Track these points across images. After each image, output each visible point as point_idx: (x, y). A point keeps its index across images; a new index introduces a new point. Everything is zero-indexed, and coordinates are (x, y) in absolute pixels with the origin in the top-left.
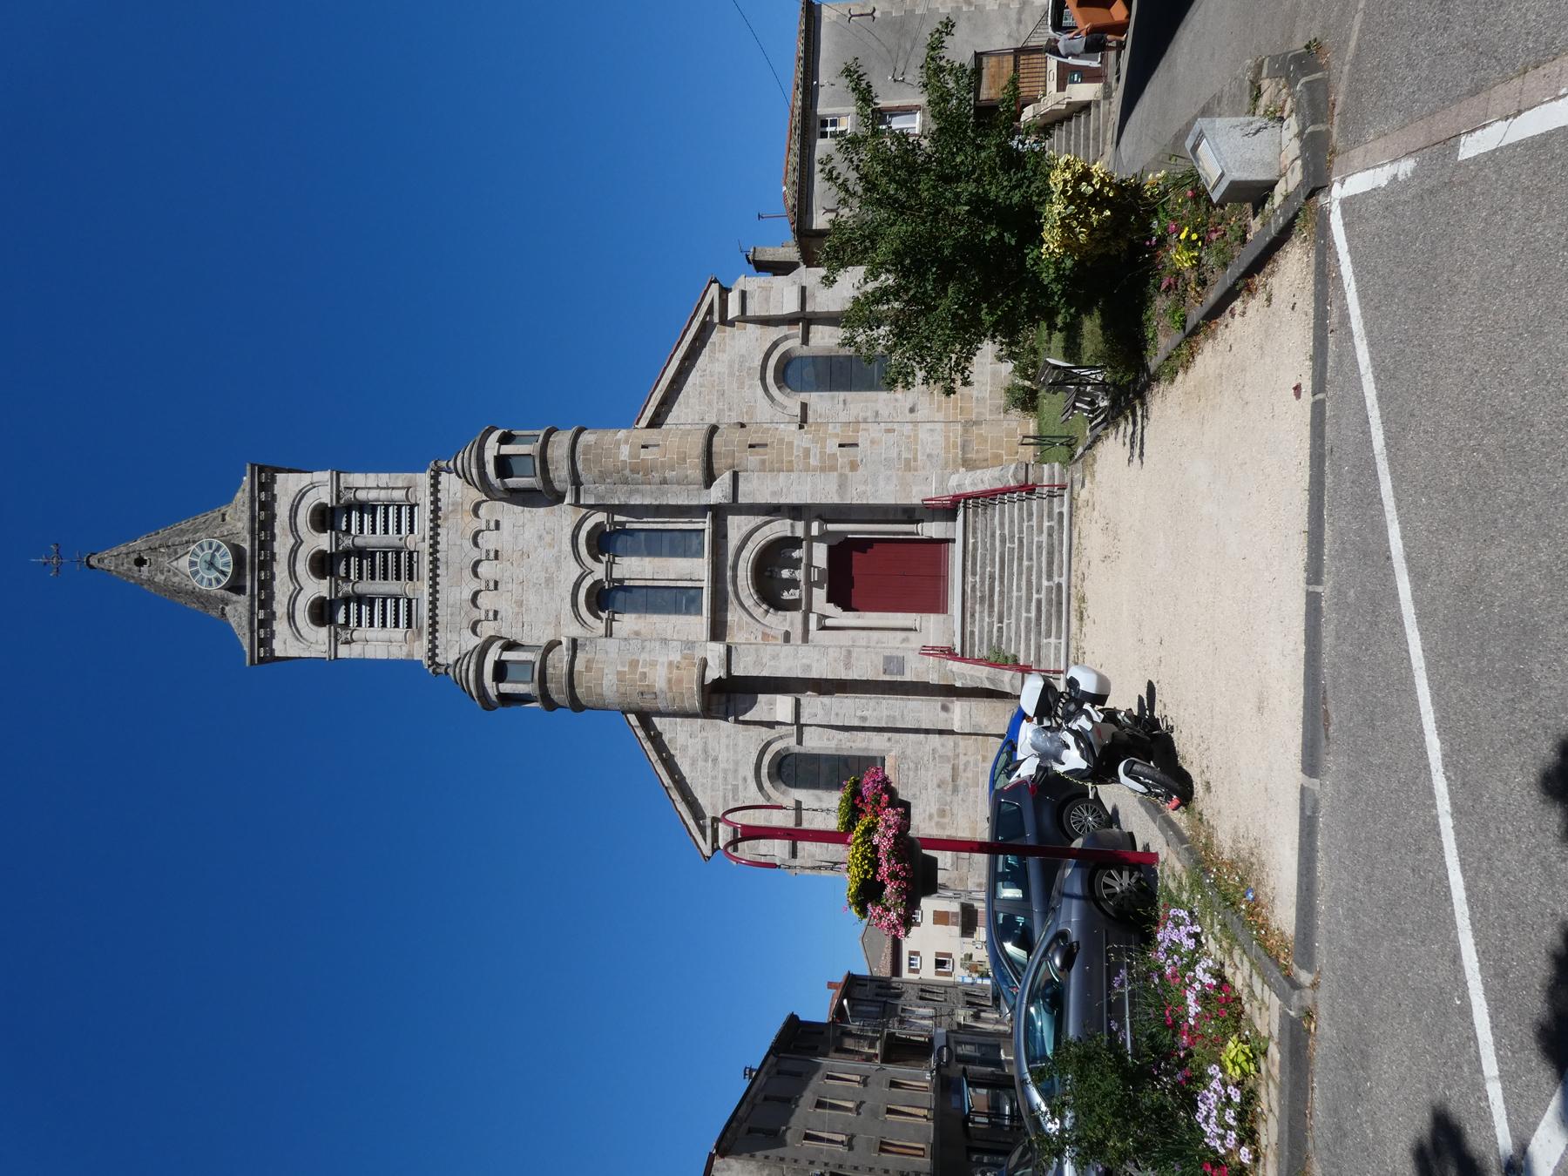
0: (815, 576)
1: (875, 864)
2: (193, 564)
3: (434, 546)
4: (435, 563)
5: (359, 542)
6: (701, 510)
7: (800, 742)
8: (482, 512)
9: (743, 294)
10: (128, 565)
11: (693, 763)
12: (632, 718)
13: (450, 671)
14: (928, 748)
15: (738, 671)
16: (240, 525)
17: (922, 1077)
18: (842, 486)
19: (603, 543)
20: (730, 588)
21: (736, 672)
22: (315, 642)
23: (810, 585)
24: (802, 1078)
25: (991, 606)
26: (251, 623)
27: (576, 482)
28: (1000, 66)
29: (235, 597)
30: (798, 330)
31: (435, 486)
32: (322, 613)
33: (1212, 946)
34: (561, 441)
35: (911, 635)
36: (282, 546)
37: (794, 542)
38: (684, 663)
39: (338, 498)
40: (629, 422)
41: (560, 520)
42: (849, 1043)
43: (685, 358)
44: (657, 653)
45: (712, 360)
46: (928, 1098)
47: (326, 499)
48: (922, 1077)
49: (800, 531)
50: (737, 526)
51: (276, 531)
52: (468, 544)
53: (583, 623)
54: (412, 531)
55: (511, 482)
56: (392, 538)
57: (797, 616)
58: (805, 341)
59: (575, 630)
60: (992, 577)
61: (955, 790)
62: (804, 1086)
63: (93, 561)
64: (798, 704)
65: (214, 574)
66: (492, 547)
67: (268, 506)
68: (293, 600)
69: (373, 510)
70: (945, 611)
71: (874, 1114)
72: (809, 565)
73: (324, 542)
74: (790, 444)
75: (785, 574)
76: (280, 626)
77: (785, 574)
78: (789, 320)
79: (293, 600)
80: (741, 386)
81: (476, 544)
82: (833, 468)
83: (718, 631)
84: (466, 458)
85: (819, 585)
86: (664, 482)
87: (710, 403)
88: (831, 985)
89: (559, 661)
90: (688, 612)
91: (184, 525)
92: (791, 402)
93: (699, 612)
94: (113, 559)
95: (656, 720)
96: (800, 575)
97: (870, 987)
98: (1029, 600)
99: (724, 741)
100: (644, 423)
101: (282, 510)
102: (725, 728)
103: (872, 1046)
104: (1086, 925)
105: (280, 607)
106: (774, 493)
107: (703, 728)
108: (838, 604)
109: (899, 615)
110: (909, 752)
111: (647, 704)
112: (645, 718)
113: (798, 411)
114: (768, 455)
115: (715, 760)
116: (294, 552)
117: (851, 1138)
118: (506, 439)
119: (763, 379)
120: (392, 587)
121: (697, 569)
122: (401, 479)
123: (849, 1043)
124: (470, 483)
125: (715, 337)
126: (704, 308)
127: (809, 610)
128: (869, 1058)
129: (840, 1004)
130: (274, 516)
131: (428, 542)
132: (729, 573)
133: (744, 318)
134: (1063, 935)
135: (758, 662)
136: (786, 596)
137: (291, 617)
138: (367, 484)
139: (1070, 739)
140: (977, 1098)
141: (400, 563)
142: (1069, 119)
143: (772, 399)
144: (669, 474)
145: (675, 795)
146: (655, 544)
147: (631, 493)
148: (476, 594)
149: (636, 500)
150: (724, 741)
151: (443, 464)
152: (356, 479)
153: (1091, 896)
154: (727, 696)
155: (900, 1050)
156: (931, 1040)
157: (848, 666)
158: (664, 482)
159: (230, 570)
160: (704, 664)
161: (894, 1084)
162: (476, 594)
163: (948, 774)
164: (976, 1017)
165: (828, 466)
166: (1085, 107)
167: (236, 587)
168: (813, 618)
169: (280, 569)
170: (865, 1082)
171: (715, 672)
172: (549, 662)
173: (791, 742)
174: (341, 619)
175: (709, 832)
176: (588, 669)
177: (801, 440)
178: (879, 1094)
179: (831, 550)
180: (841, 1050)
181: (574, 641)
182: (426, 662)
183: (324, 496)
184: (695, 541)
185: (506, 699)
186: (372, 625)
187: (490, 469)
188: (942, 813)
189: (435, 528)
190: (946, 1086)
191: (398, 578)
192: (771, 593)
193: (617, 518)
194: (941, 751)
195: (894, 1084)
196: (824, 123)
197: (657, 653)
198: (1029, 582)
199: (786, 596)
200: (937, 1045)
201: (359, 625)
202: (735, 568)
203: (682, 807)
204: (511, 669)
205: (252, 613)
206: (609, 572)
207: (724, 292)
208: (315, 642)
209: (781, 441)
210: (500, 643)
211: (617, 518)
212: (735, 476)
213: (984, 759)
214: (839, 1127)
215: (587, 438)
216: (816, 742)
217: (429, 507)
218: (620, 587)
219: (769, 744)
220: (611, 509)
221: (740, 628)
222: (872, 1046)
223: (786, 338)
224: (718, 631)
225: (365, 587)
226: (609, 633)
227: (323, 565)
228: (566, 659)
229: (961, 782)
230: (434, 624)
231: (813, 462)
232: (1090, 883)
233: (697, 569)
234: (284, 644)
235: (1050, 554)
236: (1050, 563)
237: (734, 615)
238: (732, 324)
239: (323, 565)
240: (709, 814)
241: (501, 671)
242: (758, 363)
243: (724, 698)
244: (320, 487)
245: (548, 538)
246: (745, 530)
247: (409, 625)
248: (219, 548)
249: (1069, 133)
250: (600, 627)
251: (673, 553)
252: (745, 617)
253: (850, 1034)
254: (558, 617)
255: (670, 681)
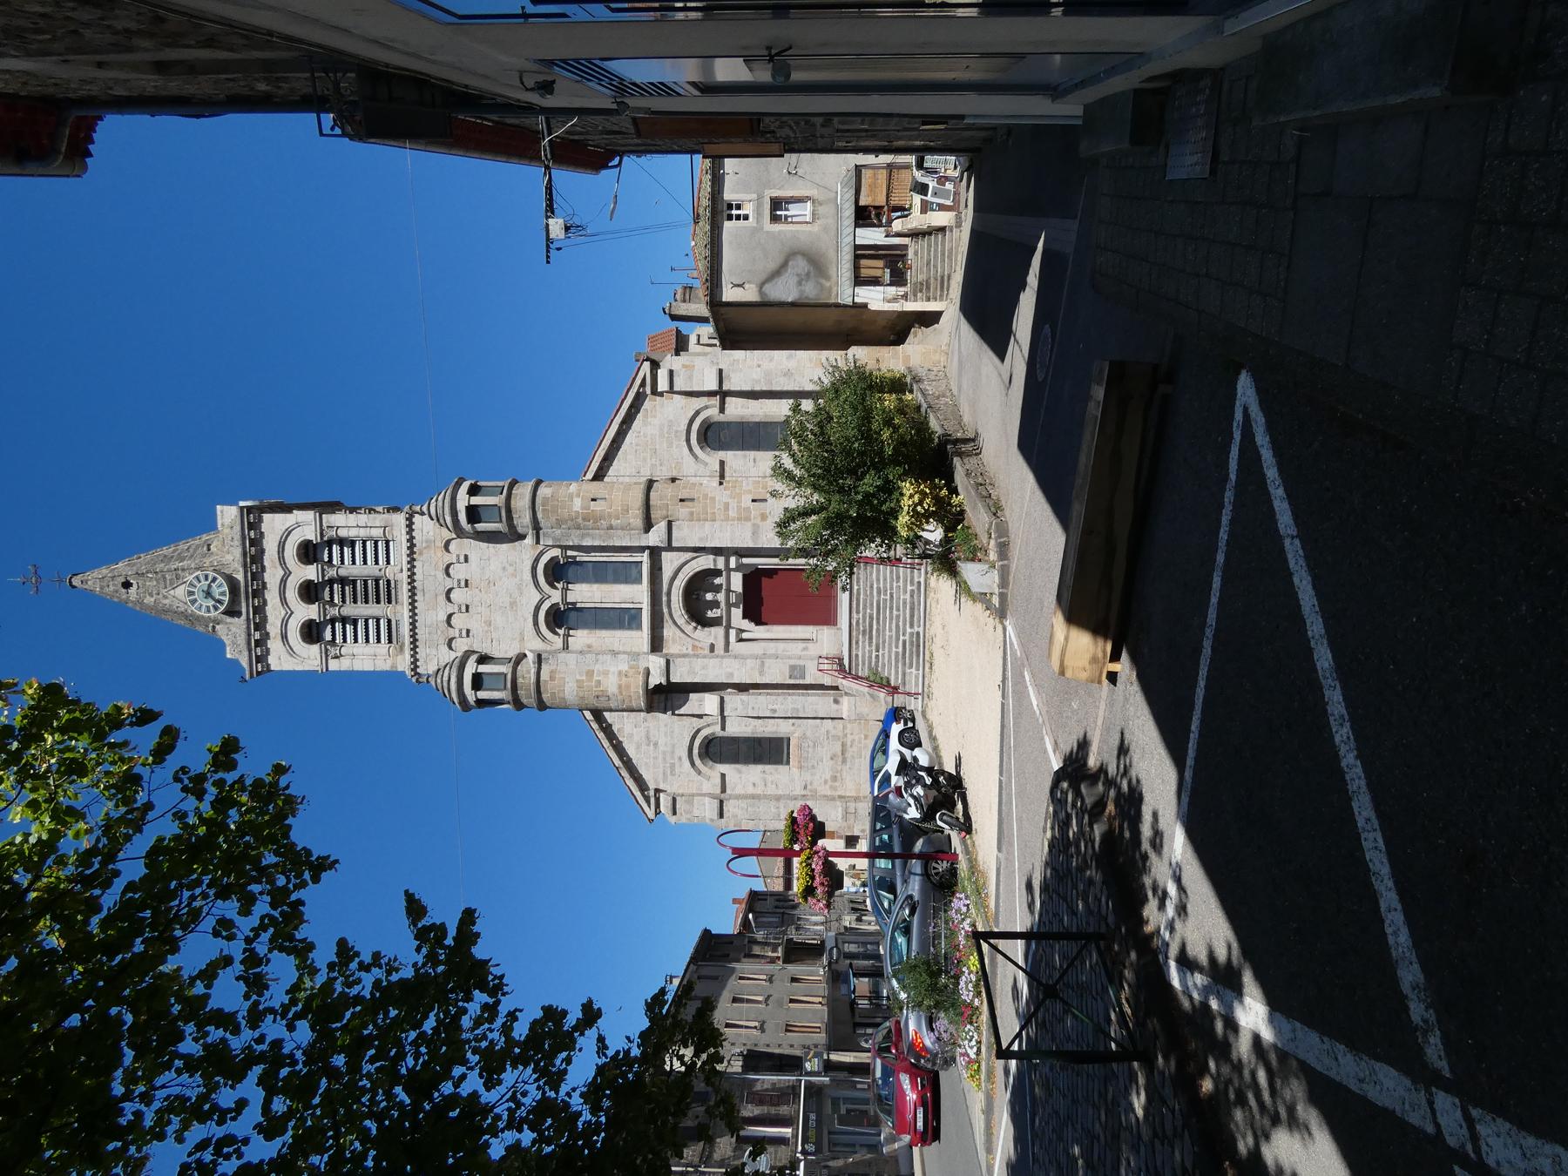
0: (733, 599)
1: (813, 878)
2: (191, 593)
3: (412, 576)
4: (413, 591)
5: (343, 572)
6: (642, 549)
7: (723, 728)
8: (452, 547)
9: (671, 373)
10: (114, 587)
11: (638, 747)
12: (588, 714)
13: (432, 681)
14: (823, 730)
15: (675, 679)
16: (229, 557)
17: (816, 972)
18: (755, 533)
19: (557, 572)
20: (665, 610)
21: (673, 680)
22: (309, 657)
23: (729, 606)
24: (720, 981)
25: (871, 638)
26: (249, 643)
27: (537, 527)
28: (875, 176)
29: (229, 619)
30: (716, 401)
31: (410, 526)
32: (311, 632)
33: (973, 911)
34: (523, 493)
35: (810, 645)
36: (272, 576)
37: (718, 573)
38: (631, 672)
39: (322, 535)
40: (576, 476)
41: (522, 553)
42: (757, 950)
43: (623, 422)
44: (607, 663)
45: (645, 424)
46: (823, 989)
47: (311, 537)
48: (816, 972)
49: (721, 563)
50: (669, 561)
51: (266, 563)
52: (441, 575)
53: (544, 639)
54: (388, 562)
55: (480, 527)
56: (371, 569)
57: (718, 632)
58: (722, 410)
59: (538, 645)
60: (871, 618)
61: (844, 761)
62: (723, 987)
63: (76, 581)
64: (722, 700)
65: (211, 603)
66: (462, 577)
67: (257, 542)
68: (285, 623)
69: (352, 544)
70: (835, 624)
71: (780, 1004)
72: (729, 590)
73: (311, 572)
74: (713, 499)
75: (709, 596)
76: (275, 645)
77: (709, 596)
78: (711, 394)
79: (285, 623)
80: (670, 445)
81: (448, 575)
82: (748, 519)
83: (656, 645)
84: (440, 502)
85: (736, 605)
86: (611, 527)
87: (645, 459)
88: (735, 901)
89: (528, 669)
90: (630, 628)
91: (166, 551)
92: (712, 459)
93: (639, 627)
94: (95, 580)
95: (606, 714)
96: (721, 597)
97: (770, 902)
98: (898, 639)
99: (663, 729)
100: (590, 475)
101: (270, 545)
102: (664, 718)
103: (775, 950)
104: (923, 890)
105: (273, 627)
106: (701, 539)
107: (645, 720)
108: (751, 620)
109: (800, 628)
110: (808, 734)
111: (599, 705)
112: (598, 714)
113: (717, 467)
114: (696, 508)
115: (656, 744)
116: (283, 582)
117: (763, 1023)
118: (474, 490)
119: (688, 440)
120: (372, 609)
121: (637, 594)
122: (378, 519)
123: (757, 950)
124: (443, 524)
125: (647, 404)
126: (638, 381)
127: (728, 627)
128: (773, 961)
129: (745, 918)
130: (263, 551)
131: (405, 574)
132: (664, 599)
133: (671, 391)
134: (911, 897)
135: (692, 672)
136: (710, 614)
137: (284, 637)
138: (343, 523)
139: (911, 801)
140: (862, 985)
141: (382, 591)
142: (930, 234)
143: (696, 457)
144: (614, 522)
145: (624, 773)
146: (601, 573)
147: (583, 536)
148: (450, 616)
149: (587, 542)
150: (663, 729)
151: (418, 508)
152: (1435, 1039)
153: (926, 874)
154: (666, 697)
155: (798, 952)
156: (823, 942)
157: (761, 673)
158: (611, 527)
159: (226, 599)
160: (648, 673)
161: (794, 980)
162: (450, 616)
163: (838, 749)
164: (859, 920)
165: (744, 517)
166: (942, 229)
167: (232, 612)
168: (733, 633)
169: (272, 596)
170: (770, 980)
171: (657, 679)
172: (519, 673)
173: (717, 729)
174: (328, 636)
175: (652, 800)
176: (552, 678)
177: (721, 495)
178: (783, 988)
179: (745, 577)
180: (750, 955)
181: (539, 656)
182: (409, 673)
183: (310, 534)
184: (634, 572)
185: (481, 703)
186: (356, 641)
187: (462, 517)
188: (834, 779)
189: (412, 561)
190: (836, 978)
191: (378, 602)
192: (698, 613)
193: (570, 553)
194: (833, 732)
195: (794, 980)
196: (730, 207)
197: (607, 663)
198: (897, 626)
199: (710, 614)
200: (828, 945)
201: (345, 640)
202: (669, 594)
203: (630, 783)
204: (486, 681)
205: (249, 635)
206: (564, 597)
207: (655, 365)
208: (309, 657)
209: (705, 497)
210: (474, 657)
211: (570, 553)
212: (670, 524)
213: (866, 737)
214: (753, 1016)
215: (544, 491)
216: (735, 728)
217: (405, 544)
218: (574, 608)
219: (698, 731)
220: (565, 548)
221: (674, 641)
222: (775, 950)
223: (706, 407)
224: (656, 645)
225: (349, 610)
226: (566, 647)
227: (310, 592)
228: (533, 670)
229: (848, 755)
230: (414, 642)
231: (732, 513)
232: (926, 867)
233: (637, 594)
234: (279, 660)
235: (912, 609)
236: (912, 616)
237: (669, 631)
238: (661, 394)
239: (310, 592)
240: (652, 786)
241: (478, 681)
242: (684, 427)
243: (663, 697)
244: (305, 525)
245: (510, 570)
246: (677, 564)
247: (390, 641)
248: (214, 579)
249: (929, 245)
250: (558, 642)
251: (616, 581)
252: (678, 632)
253: (756, 942)
254: (522, 634)
255: (620, 687)
